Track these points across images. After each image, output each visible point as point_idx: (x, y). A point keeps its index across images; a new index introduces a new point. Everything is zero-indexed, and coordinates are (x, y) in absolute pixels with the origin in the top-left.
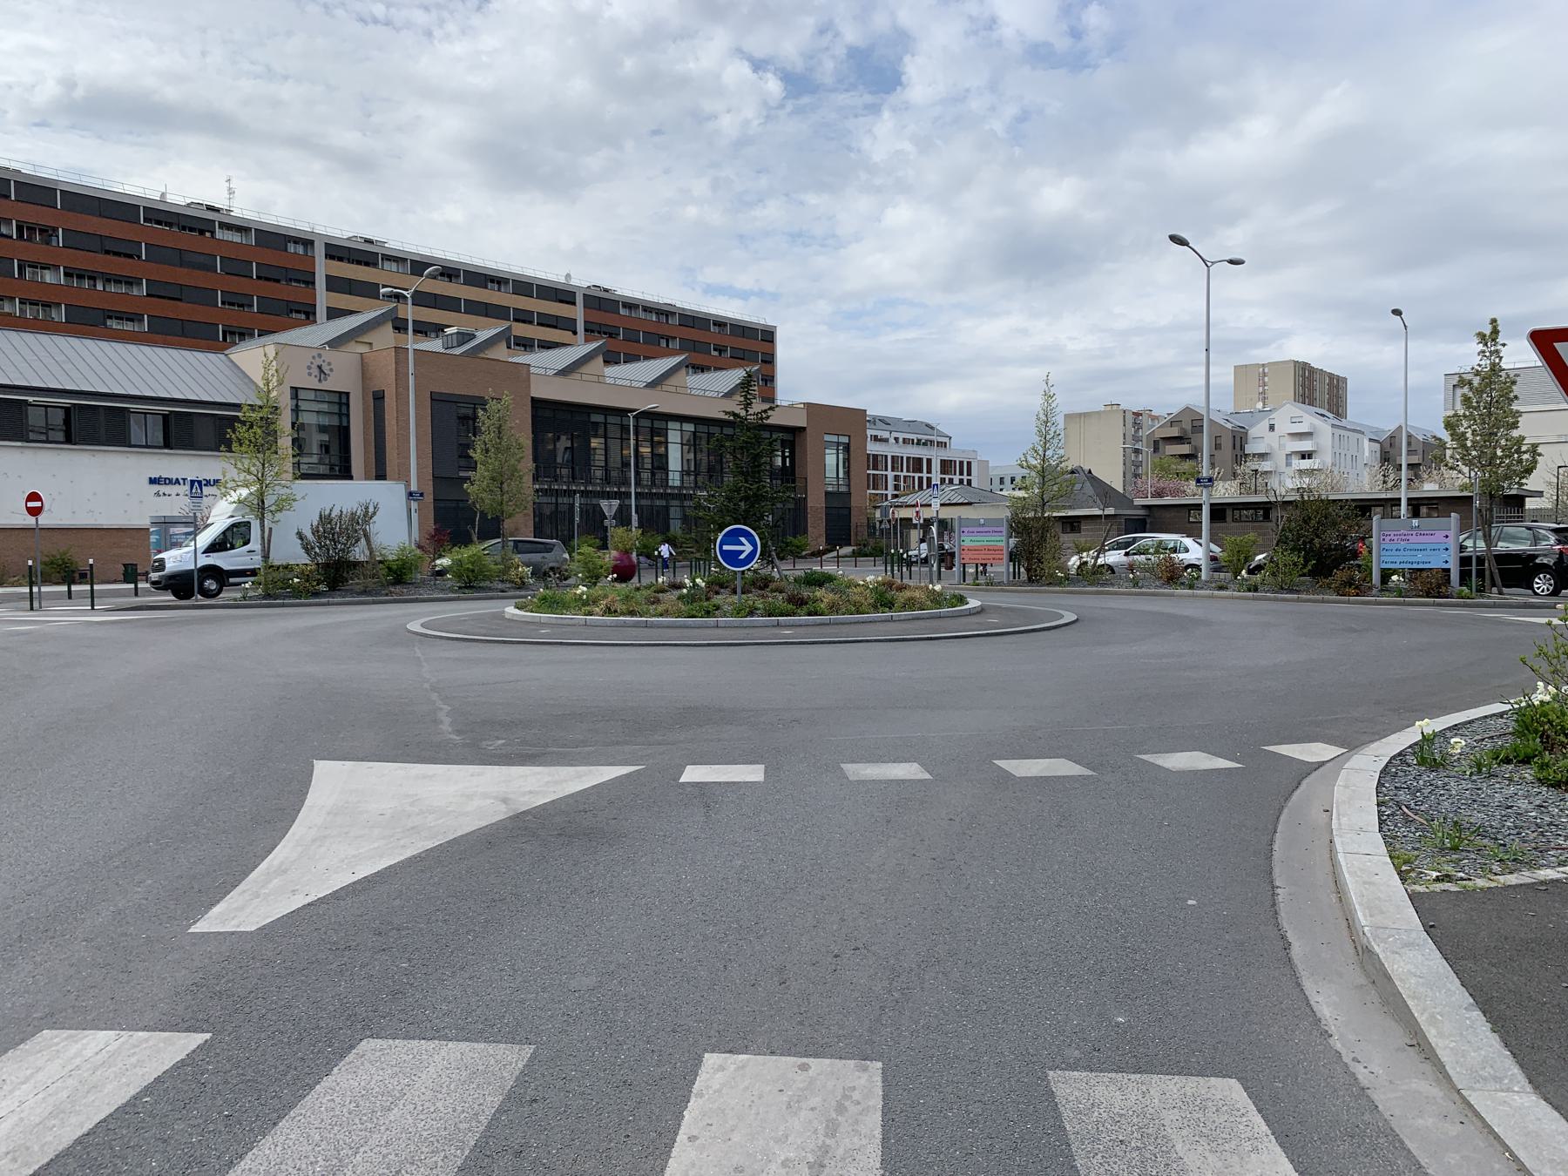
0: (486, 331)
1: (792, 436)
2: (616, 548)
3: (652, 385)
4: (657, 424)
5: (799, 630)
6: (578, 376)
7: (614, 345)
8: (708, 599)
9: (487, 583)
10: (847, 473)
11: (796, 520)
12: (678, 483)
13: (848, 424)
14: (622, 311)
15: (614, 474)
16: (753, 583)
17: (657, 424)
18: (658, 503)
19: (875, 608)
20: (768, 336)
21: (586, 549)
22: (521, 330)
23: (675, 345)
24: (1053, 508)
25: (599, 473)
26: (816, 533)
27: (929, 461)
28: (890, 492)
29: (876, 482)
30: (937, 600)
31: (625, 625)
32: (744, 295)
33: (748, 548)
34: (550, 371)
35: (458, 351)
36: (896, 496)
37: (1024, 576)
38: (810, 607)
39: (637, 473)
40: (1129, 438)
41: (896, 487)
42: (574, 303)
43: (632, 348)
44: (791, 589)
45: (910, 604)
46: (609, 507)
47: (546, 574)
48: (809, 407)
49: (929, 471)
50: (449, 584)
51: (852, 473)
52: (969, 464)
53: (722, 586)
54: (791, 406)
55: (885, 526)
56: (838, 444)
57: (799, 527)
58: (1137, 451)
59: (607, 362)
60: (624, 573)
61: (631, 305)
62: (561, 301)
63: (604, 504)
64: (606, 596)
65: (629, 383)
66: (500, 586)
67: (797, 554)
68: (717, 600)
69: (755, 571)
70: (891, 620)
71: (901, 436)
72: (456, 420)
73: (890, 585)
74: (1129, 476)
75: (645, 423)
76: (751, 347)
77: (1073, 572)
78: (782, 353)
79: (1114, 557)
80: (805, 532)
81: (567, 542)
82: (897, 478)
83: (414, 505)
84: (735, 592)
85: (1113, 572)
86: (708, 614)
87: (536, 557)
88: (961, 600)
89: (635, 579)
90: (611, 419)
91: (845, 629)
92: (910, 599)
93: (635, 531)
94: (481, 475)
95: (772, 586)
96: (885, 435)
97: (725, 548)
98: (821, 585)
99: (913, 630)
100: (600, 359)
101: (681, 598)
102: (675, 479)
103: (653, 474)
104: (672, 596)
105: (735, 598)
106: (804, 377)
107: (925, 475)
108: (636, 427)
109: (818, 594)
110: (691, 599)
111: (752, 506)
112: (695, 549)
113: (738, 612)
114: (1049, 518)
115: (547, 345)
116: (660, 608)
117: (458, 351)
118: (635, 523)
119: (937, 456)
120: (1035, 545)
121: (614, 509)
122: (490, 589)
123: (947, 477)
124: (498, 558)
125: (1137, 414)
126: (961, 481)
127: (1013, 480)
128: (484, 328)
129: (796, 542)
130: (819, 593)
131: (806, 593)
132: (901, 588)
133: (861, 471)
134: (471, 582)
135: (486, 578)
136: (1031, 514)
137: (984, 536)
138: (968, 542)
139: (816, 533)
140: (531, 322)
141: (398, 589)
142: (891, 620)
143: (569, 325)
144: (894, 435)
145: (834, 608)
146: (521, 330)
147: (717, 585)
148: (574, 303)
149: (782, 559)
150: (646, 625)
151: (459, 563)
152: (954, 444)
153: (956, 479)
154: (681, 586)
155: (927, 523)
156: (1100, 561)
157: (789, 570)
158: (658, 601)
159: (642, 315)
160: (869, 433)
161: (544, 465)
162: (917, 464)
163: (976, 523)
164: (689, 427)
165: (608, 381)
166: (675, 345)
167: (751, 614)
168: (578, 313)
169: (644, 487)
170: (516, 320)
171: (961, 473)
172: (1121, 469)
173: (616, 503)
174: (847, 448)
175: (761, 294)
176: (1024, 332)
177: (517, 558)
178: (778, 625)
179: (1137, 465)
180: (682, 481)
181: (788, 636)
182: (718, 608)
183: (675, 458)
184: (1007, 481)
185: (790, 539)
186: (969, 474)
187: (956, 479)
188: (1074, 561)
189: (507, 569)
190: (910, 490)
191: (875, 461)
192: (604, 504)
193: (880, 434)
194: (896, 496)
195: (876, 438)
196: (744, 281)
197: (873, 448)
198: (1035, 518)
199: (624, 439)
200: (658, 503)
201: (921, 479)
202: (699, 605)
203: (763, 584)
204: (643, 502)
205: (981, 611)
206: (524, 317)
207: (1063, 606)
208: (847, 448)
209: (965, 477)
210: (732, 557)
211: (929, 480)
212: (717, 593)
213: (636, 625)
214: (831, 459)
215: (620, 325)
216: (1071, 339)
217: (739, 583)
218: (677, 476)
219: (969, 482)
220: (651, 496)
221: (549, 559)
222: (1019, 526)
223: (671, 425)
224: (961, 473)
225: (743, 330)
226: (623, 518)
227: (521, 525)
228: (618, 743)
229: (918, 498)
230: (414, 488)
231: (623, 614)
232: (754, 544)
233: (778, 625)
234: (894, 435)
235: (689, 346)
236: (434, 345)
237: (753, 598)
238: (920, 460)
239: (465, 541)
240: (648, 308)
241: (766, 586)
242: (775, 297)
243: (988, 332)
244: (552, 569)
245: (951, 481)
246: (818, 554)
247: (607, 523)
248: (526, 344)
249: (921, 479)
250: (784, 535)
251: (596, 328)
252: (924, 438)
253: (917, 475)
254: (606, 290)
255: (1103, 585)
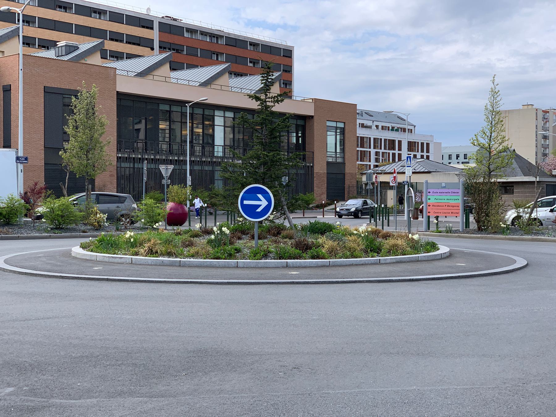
0: (86, 44)
1: (303, 122)
2: (173, 201)
3: (205, 84)
4: (207, 112)
5: (304, 271)
6: (151, 77)
7: (179, 58)
8: (231, 243)
9: (73, 226)
10: (343, 150)
11: (306, 181)
12: (220, 154)
13: (344, 115)
14: (186, 35)
15: (175, 147)
16: (269, 231)
17: (207, 112)
18: (206, 168)
19: (366, 252)
20: (288, 53)
21: (150, 201)
22: (111, 46)
23: (223, 58)
24: (496, 176)
25: (165, 147)
26: (320, 191)
27: (400, 142)
28: (373, 163)
29: (363, 156)
30: (415, 247)
31: (163, 264)
32: (273, 27)
33: (264, 203)
34: (131, 75)
35: (66, 58)
36: (376, 166)
37: (473, 225)
38: (313, 251)
39: (192, 147)
40: (540, 128)
41: (377, 160)
42: (152, 28)
43: (192, 60)
44: (299, 236)
45: (394, 250)
46: (166, 170)
47: (119, 220)
48: (316, 102)
49: (400, 149)
50: (45, 226)
51: (347, 149)
52: (428, 144)
53: (244, 232)
54: (303, 101)
55: (370, 187)
56: (336, 128)
57: (308, 187)
58: (545, 137)
59: (173, 69)
60: (176, 219)
61: (192, 31)
62: (143, 27)
63: (162, 168)
64: (149, 240)
65: (187, 84)
66: (83, 228)
67: (306, 206)
68: (239, 244)
69: (271, 221)
70: (379, 263)
71: (380, 125)
72: (58, 103)
73: (376, 233)
74: (540, 155)
75: (199, 111)
76: (274, 62)
77: (509, 223)
78: (298, 67)
79: (542, 213)
80: (312, 190)
81: (138, 198)
82: (377, 154)
83: (21, 167)
84: (253, 237)
85: (542, 224)
86: (230, 256)
87: (112, 207)
88: (434, 246)
89: (187, 223)
90: (174, 108)
91: (341, 270)
92: (395, 246)
93: (188, 190)
94: (71, 145)
95: (284, 233)
96: (369, 123)
97: (246, 202)
98: (323, 233)
99: (398, 271)
100: (167, 66)
101: (210, 242)
102: (219, 151)
103: (203, 148)
104: (202, 241)
105: (253, 243)
106: (313, 81)
107: (397, 152)
108: (192, 115)
109: (320, 241)
110: (217, 243)
111: (269, 169)
112: (222, 203)
113: (255, 255)
114: (494, 183)
115: (130, 56)
116: (193, 250)
117: (66, 58)
118: (189, 183)
119: (405, 139)
120: (484, 200)
121: (170, 171)
122: (74, 230)
123: (413, 153)
124: (83, 207)
125: (546, 112)
126: (422, 157)
127: (458, 156)
128: (84, 42)
129: (305, 197)
130: (321, 240)
131: (310, 240)
132: (386, 236)
133: (352, 148)
134: (61, 225)
135: (75, 222)
136: (481, 180)
137: (444, 196)
138: (433, 199)
139: (320, 191)
140: (121, 41)
141: (5, 229)
142: (379, 263)
143: (148, 44)
144: (376, 123)
145: (332, 253)
146: (111, 46)
147: (241, 232)
148: (152, 28)
149: (292, 212)
150: (180, 265)
151: (52, 210)
152: (417, 130)
153: (419, 155)
154: (211, 232)
155: (401, 186)
156: (534, 215)
157: (299, 220)
158: (191, 244)
159: (200, 37)
160: (359, 121)
161: (124, 141)
162: (391, 144)
163: (438, 185)
164: (230, 114)
165: (172, 80)
166: (224, 58)
167: (265, 256)
168: (155, 35)
169: (196, 156)
170: (112, 39)
171: (422, 151)
172: (534, 150)
173: (171, 167)
174: (343, 131)
175: (285, 27)
176: (466, 55)
177: (96, 208)
178: (287, 266)
179: (546, 147)
180: (224, 152)
181: (292, 277)
182: (238, 251)
183: (219, 137)
184: (454, 157)
185: (301, 195)
186: (428, 151)
187: (419, 155)
188: (511, 214)
189: (89, 215)
190: (386, 162)
191: (362, 141)
192: (162, 168)
193: (366, 123)
194: (376, 166)
195: (363, 126)
196: (274, 18)
197: (361, 132)
198: (482, 184)
199: (184, 123)
200: (206, 168)
201: (394, 155)
202: (224, 248)
203: (276, 231)
204: (197, 168)
205: (449, 256)
206: (116, 37)
207: (513, 251)
208: (343, 131)
209: (425, 154)
210: (251, 211)
211: (400, 155)
212: (239, 238)
213: (172, 264)
214: (331, 139)
215: (182, 44)
216: (499, 60)
217: (256, 231)
218: (221, 149)
219: (428, 157)
220: (202, 163)
221: (123, 208)
222: (470, 189)
223: (217, 113)
224: (422, 151)
225: (270, 49)
226: (178, 178)
227: (106, 180)
228: (121, 394)
229: (396, 166)
230: (21, 154)
231: (162, 255)
232: (269, 200)
233: (287, 266)
234: (376, 123)
235: (230, 58)
236: (50, 54)
237: (268, 244)
238: (394, 141)
239: (59, 195)
240: (204, 33)
241: (279, 233)
242: (295, 28)
243: (442, 54)
244: (122, 216)
245: (415, 156)
246: (321, 206)
247: (164, 182)
248: (117, 56)
249: (394, 155)
250: (297, 192)
251: (168, 46)
252: (396, 126)
253: (391, 152)
254: (175, 20)
255: (536, 234)
